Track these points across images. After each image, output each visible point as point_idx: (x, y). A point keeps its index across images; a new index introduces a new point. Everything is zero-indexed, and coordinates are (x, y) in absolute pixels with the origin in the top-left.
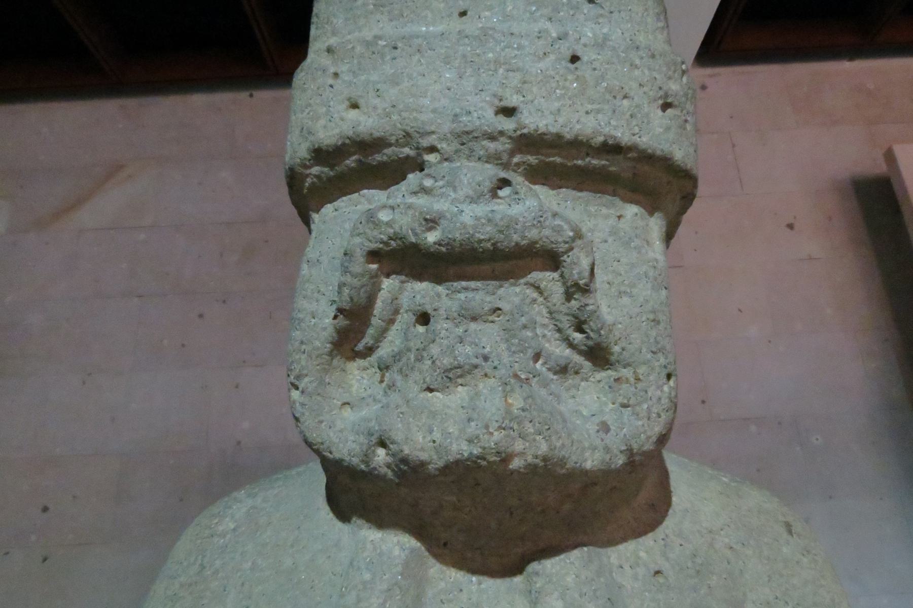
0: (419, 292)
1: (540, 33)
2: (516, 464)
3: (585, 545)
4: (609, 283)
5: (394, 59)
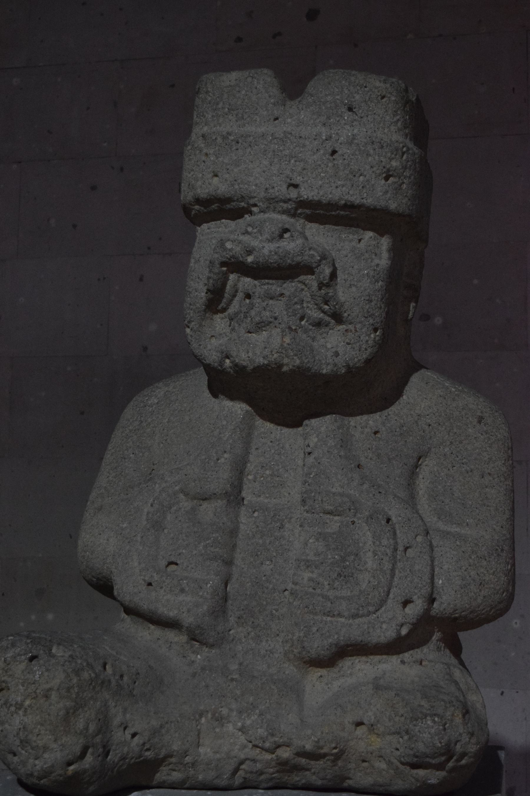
0: (247, 283)
1: (316, 136)
2: (285, 369)
3: (334, 414)
4: (345, 280)
5: (237, 149)
